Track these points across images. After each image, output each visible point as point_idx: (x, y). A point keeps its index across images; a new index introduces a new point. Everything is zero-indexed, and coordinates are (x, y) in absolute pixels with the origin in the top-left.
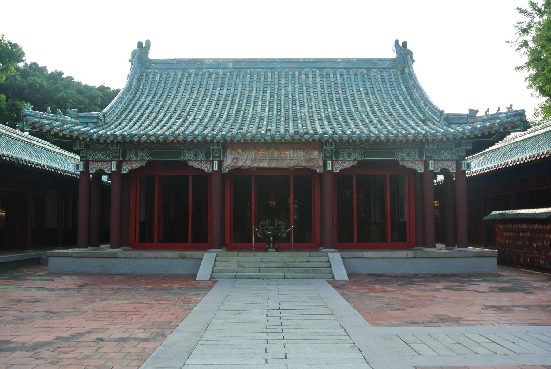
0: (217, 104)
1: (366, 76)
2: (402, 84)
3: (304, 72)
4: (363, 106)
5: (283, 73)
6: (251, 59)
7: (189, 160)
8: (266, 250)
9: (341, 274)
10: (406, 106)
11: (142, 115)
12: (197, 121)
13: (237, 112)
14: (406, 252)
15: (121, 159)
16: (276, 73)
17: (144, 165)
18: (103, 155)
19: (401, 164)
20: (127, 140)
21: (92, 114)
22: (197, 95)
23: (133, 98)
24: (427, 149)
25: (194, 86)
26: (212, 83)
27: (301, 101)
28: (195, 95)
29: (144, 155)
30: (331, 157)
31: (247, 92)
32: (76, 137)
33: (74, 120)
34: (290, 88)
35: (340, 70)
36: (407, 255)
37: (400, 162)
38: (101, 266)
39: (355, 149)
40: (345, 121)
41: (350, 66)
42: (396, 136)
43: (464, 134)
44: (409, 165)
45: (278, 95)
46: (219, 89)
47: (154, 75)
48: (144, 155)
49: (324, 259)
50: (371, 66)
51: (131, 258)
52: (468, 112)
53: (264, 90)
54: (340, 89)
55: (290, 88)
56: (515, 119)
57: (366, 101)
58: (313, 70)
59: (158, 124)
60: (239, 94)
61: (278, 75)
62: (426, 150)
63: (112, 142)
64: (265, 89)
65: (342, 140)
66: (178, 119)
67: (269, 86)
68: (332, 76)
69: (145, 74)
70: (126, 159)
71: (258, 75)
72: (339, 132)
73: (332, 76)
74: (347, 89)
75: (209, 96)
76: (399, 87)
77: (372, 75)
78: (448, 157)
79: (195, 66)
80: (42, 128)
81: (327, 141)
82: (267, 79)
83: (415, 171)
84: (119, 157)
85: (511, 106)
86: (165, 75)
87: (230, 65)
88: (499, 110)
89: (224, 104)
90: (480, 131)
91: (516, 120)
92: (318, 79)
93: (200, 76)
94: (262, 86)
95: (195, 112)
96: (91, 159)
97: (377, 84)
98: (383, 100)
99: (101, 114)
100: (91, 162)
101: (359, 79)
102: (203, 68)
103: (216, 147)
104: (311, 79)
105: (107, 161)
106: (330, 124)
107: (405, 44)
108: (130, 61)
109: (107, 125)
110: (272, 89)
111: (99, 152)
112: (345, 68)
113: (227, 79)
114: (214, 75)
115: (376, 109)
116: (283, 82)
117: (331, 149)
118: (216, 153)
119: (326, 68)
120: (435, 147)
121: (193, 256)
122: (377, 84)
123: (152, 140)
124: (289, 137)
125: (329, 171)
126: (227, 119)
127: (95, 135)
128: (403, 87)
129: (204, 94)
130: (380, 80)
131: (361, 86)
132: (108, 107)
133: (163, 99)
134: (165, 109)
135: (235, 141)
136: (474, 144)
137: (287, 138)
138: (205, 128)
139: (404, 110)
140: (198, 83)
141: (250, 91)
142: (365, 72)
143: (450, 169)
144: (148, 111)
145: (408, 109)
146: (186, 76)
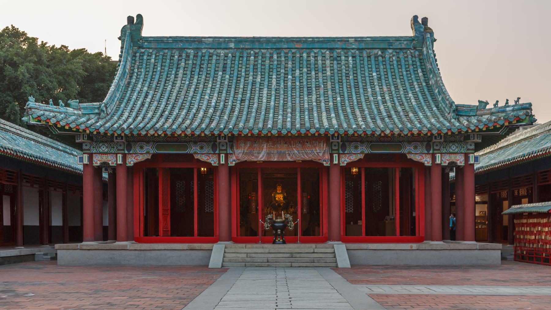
0: (220, 92)
1: (380, 58)
2: (418, 67)
4: (374, 94)
5: (290, 55)
7: (196, 153)
9: (344, 261)
10: (420, 95)
11: (143, 105)
12: (201, 113)
13: (242, 101)
15: (126, 152)
17: (150, 157)
18: (107, 147)
19: (409, 157)
21: (93, 105)
22: (198, 80)
23: (129, 83)
28: (195, 80)
29: (150, 148)
30: (338, 150)
31: (251, 78)
32: (83, 130)
33: (76, 112)
34: (298, 72)
35: (353, 51)
36: (411, 247)
37: (408, 155)
38: (111, 258)
39: (148, 142)
40: (353, 113)
41: (364, 47)
44: (417, 158)
45: (284, 81)
46: (220, 73)
47: (148, 56)
48: (150, 148)
49: (330, 250)
50: (387, 47)
51: (141, 250)
52: (477, 104)
53: (269, 75)
54: (351, 73)
55: (298, 72)
56: (521, 113)
57: (377, 88)
58: (323, 51)
59: (161, 116)
60: (242, 80)
61: (285, 57)
62: (433, 143)
63: (119, 135)
64: (271, 73)
65: (348, 134)
66: (181, 109)
68: (343, 58)
69: (138, 55)
70: (131, 152)
71: (262, 57)
72: (345, 125)
73: (343, 58)
74: (359, 74)
75: (210, 82)
76: (415, 71)
77: (387, 56)
78: (456, 150)
79: (194, 46)
80: (48, 121)
82: (273, 61)
83: (423, 164)
84: (124, 150)
85: (519, 98)
86: (161, 57)
87: (232, 45)
88: (507, 103)
89: (228, 92)
90: (485, 125)
91: (521, 113)
92: (328, 62)
93: (199, 58)
94: (267, 71)
95: (197, 101)
96: (95, 151)
97: (392, 67)
98: (396, 87)
99: (103, 105)
101: (373, 62)
102: (202, 48)
103: (222, 140)
104: (320, 62)
105: (111, 153)
106: (337, 116)
107: (425, 20)
108: (120, 38)
109: (109, 117)
110: (278, 73)
111: (103, 144)
112: (358, 49)
113: (229, 62)
114: (215, 57)
116: (290, 66)
117: (338, 143)
118: (223, 146)
119: (337, 49)
120: (442, 140)
121: (202, 248)
122: (392, 67)
123: (160, 134)
124: (296, 132)
125: (335, 164)
126: (232, 110)
127: (102, 128)
129: (206, 80)
130: (395, 62)
131: (374, 69)
132: (108, 96)
133: (162, 86)
134: (166, 97)
135: (243, 135)
136: (483, 137)
137: (294, 132)
138: (211, 121)
139: (417, 98)
140: (198, 67)
141: (255, 76)
142: (380, 53)
143: (458, 162)
144: (148, 100)
145: (421, 98)
146: (184, 57)
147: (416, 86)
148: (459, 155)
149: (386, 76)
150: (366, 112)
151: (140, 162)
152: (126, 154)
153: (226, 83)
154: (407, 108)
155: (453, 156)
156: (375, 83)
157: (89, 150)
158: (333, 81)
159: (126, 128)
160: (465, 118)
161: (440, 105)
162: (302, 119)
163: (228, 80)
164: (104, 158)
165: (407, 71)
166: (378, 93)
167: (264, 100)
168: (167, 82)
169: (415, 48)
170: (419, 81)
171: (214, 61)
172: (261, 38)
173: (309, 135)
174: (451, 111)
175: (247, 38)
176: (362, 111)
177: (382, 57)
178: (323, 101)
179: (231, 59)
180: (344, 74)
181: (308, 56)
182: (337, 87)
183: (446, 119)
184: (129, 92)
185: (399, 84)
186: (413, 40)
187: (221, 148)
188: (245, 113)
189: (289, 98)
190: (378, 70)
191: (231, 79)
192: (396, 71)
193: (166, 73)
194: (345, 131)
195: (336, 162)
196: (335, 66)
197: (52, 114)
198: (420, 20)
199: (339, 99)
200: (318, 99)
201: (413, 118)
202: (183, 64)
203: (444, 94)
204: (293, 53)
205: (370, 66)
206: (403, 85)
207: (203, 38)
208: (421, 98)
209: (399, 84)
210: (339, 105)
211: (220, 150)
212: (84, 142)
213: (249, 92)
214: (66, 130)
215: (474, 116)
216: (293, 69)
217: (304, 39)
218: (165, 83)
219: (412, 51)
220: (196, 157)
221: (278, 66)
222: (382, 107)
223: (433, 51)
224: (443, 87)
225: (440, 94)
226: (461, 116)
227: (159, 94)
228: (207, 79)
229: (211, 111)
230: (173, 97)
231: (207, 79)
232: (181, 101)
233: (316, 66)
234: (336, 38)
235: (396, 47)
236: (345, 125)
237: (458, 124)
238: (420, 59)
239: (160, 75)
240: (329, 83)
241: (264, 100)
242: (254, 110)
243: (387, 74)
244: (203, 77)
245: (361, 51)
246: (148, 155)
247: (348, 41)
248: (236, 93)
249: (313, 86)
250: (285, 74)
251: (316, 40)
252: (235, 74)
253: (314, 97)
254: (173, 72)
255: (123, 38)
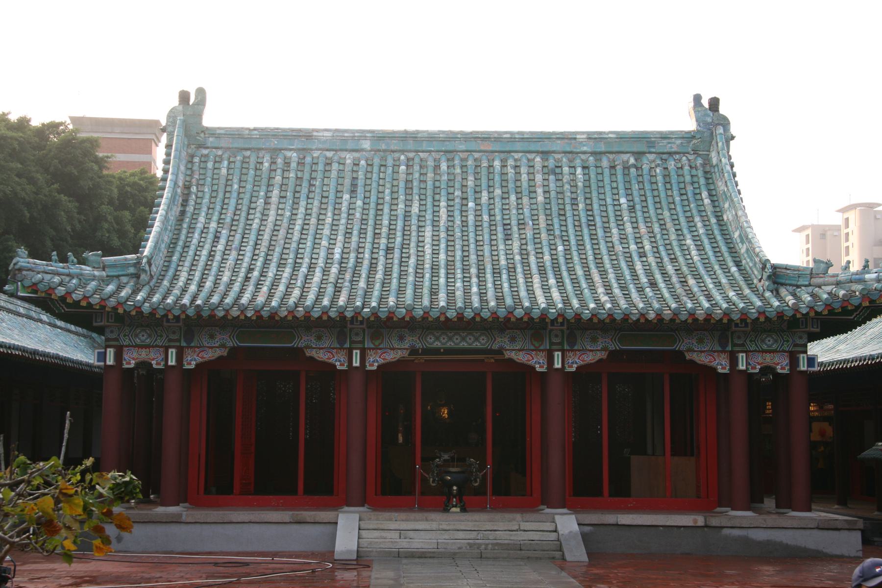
0: (348, 233)
1: (633, 171)
2: (703, 188)
3: (511, 162)
4: (623, 239)
6: (406, 132)
8: (446, 510)
11: (211, 255)
13: (389, 250)
14: (693, 517)
15: (184, 344)
16: (457, 162)
17: (225, 354)
18: (150, 336)
19: (688, 357)
20: (205, 314)
21: (126, 259)
22: (306, 209)
23: (183, 213)
24: (735, 331)
25: (298, 189)
26: (333, 184)
27: (506, 226)
28: (302, 210)
30: (561, 344)
33: (96, 273)
34: (485, 196)
35: (583, 157)
36: (695, 521)
37: (686, 354)
41: (603, 149)
42: (675, 314)
43: (797, 310)
44: (703, 359)
45: (462, 211)
46: (346, 197)
49: (549, 526)
50: (645, 149)
54: (581, 199)
55: (485, 196)
57: (629, 229)
59: (247, 279)
60: (386, 210)
61: (462, 167)
66: (281, 265)
67: (443, 193)
68: (566, 170)
69: (196, 160)
70: (192, 345)
71: (421, 167)
73: (566, 170)
74: (595, 200)
78: (774, 347)
79: (297, 145)
81: (553, 322)
83: (714, 370)
84: (179, 340)
86: (238, 165)
87: (366, 145)
89: (362, 232)
90: (826, 305)
92: (539, 178)
93: (307, 169)
94: (429, 192)
95: (308, 250)
98: (663, 226)
100: (125, 349)
102: (312, 150)
104: (524, 177)
107: (714, 103)
110: (451, 197)
112: (593, 153)
113: (361, 175)
114: (335, 166)
115: (648, 247)
116: (470, 183)
117: (562, 331)
118: (357, 334)
119: (554, 152)
121: (318, 519)
122: (654, 187)
123: (249, 315)
125: (557, 369)
126: (373, 267)
127: (147, 305)
128: (705, 194)
129: (321, 209)
131: (622, 192)
134: (251, 243)
137: (486, 314)
138: (337, 290)
139: (700, 248)
140: (305, 184)
141: (408, 203)
142: (632, 161)
143: (779, 367)
144: (220, 247)
145: (708, 247)
147: (699, 225)
148: (779, 354)
149: (644, 204)
150: (611, 276)
151: (206, 362)
152: (183, 347)
153: (358, 215)
154: (685, 269)
155: (768, 356)
156: (625, 219)
157: (116, 340)
158: (548, 212)
159: (188, 304)
160: (791, 289)
161: (744, 262)
162: (498, 287)
163: (360, 210)
164: (143, 355)
165: (682, 195)
166: (631, 238)
167: (428, 250)
168: (251, 211)
169: (695, 151)
170: (704, 214)
171: (334, 174)
172: (418, 132)
173: (513, 319)
174: (765, 277)
175: (394, 132)
176: (603, 273)
177: (637, 169)
178: (533, 253)
179: (364, 170)
180: (568, 200)
181: (504, 166)
182: (556, 226)
183: (754, 290)
184: (184, 232)
185: (668, 220)
186: (694, 137)
187: (355, 339)
188: (395, 275)
189: (472, 246)
190: (629, 192)
191: (366, 206)
192: (663, 195)
193: (248, 196)
194: (576, 314)
195: (558, 365)
196: (552, 186)
197: (57, 279)
198: (705, 103)
199: (560, 248)
200: (524, 247)
201: (695, 289)
202: (278, 179)
203: (750, 242)
204: (475, 160)
205: (614, 185)
206: (675, 220)
207: (314, 130)
208: (708, 247)
209: (668, 220)
210: (562, 260)
211: (352, 342)
212: (108, 326)
213: (399, 234)
214: (83, 307)
215: (806, 286)
216: (478, 189)
217: (496, 135)
218: (248, 214)
219: (691, 157)
220: (307, 354)
221: (451, 184)
222: (639, 267)
223: (730, 158)
224: (748, 230)
225: (742, 242)
226: (782, 284)
227: (238, 237)
228: (323, 206)
229: (334, 270)
230: (265, 243)
231: (323, 206)
232: (278, 249)
233: (518, 184)
234: (554, 133)
235: (661, 151)
236: (575, 303)
237: (776, 303)
238: (706, 172)
239: (239, 198)
240: (542, 218)
241: (428, 250)
242: (411, 270)
243: (646, 201)
244: (316, 203)
245: (598, 157)
246: (223, 350)
247: (575, 139)
248: (376, 235)
249: (514, 222)
250: (463, 199)
251: (517, 136)
252: (373, 198)
253: (516, 245)
254: (262, 194)
255: (170, 129)
